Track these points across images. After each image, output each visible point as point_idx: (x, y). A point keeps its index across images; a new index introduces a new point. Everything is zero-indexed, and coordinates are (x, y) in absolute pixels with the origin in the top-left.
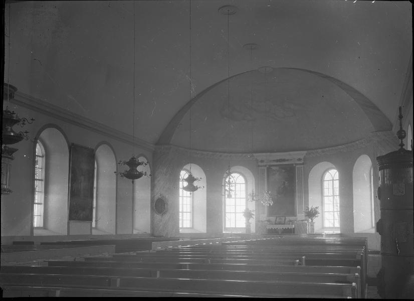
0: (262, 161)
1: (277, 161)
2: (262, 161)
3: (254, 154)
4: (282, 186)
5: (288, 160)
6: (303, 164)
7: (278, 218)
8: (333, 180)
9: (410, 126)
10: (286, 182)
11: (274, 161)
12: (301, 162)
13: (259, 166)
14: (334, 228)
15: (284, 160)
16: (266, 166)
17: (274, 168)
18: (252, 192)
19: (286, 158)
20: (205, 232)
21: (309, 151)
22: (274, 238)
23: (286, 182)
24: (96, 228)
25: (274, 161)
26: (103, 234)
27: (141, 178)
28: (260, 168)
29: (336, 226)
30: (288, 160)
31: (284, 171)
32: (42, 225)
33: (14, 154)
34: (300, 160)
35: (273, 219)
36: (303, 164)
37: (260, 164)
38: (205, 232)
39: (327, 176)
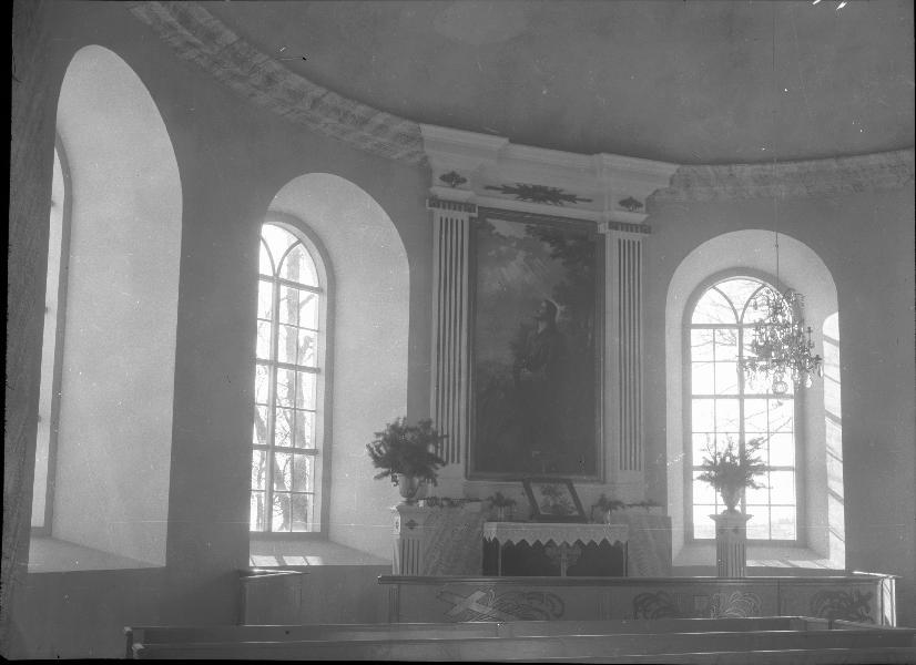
0: (629, 203)
1: (525, 192)
2: (453, 179)
3: (429, 131)
4: (542, 327)
5: (572, 198)
6: (644, 228)
10: (560, 308)
11: (507, 190)
12: (638, 217)
13: (436, 202)
15: (553, 196)
16: (468, 207)
17: (502, 227)
18: (754, 382)
19: (566, 186)
20: (157, 558)
21: (687, 169)
23: (560, 308)
24: (47, 532)
25: (507, 190)
26: (78, 564)
28: (439, 213)
30: (572, 198)
31: (548, 248)
32: (318, 529)
34: (629, 203)
36: (644, 228)
37: (443, 191)
38: (157, 558)
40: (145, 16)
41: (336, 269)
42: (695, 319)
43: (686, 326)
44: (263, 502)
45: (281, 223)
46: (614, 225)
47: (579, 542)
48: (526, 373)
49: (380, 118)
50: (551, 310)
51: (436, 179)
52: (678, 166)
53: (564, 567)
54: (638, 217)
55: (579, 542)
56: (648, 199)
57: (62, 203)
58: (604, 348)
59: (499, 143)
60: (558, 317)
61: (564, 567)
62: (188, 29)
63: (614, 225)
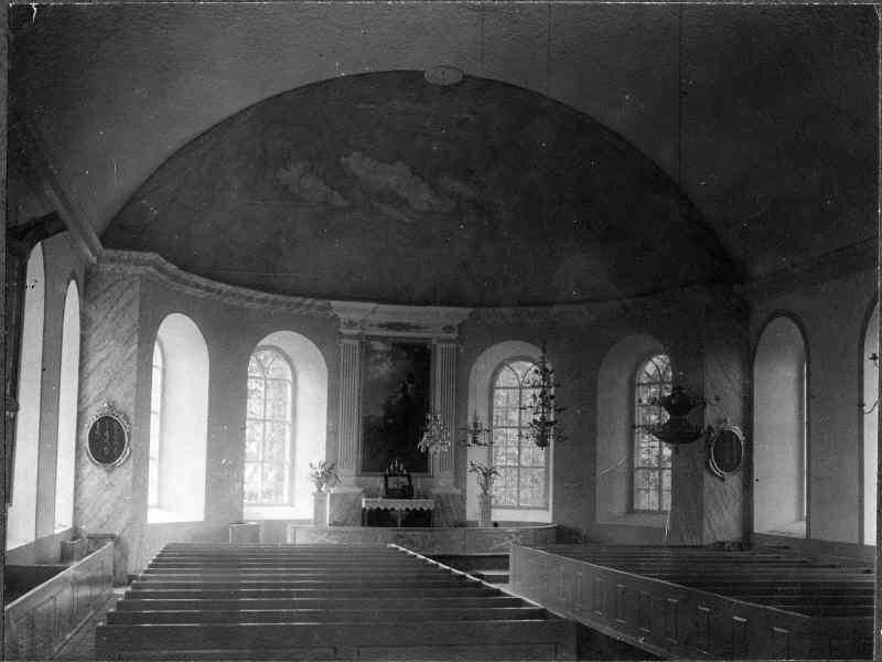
1: (391, 326)
2: (351, 324)
3: (333, 303)
4: (400, 396)
5: (417, 328)
7: (391, 480)
8: (521, 388)
9: (73, 283)
10: (410, 386)
11: (381, 326)
12: (454, 335)
14: (487, 504)
15: (406, 327)
22: (384, 540)
25: (381, 326)
27: (294, 74)
28: (345, 341)
29: (494, 511)
30: (417, 328)
31: (404, 355)
33: (457, 81)
35: (378, 482)
39: (505, 377)
40: (731, 599)
41: (186, 141)
42: (498, 384)
43: (492, 388)
44: (165, 652)
45: (255, 575)
46: (439, 341)
47: (408, 510)
48: (391, 421)
49: (309, 301)
50: (405, 386)
51: (342, 326)
52: (470, 310)
53: (399, 522)
54: (454, 335)
55: (408, 510)
56: (460, 326)
57: (266, 294)
58: (837, 584)
59: (371, 305)
60: (409, 391)
61: (399, 522)
62: (579, 624)
63: (439, 341)
